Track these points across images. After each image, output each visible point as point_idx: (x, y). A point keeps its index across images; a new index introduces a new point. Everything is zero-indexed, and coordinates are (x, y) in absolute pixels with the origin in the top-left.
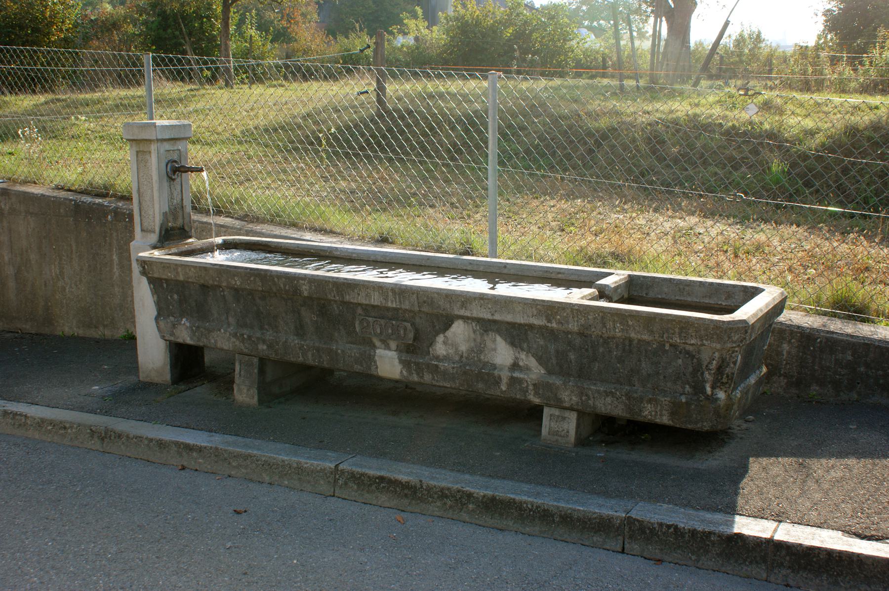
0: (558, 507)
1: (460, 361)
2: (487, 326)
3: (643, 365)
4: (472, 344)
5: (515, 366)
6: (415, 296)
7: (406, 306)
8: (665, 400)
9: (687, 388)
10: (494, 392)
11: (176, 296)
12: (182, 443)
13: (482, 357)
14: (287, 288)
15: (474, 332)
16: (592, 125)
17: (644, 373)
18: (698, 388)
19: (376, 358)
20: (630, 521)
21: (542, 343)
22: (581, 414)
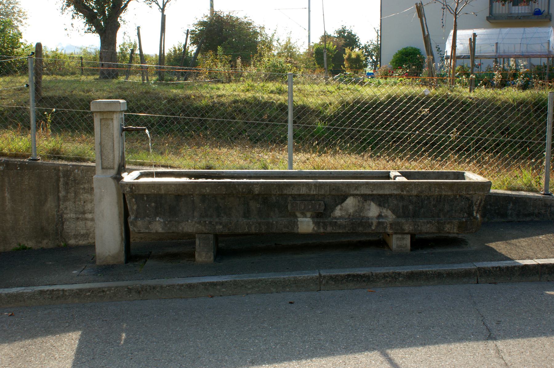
0: (445, 270)
1: (349, 218)
2: (366, 198)
3: (446, 207)
4: (357, 208)
5: (380, 216)
6: (328, 187)
7: (322, 192)
8: (456, 222)
9: (466, 215)
10: (368, 231)
11: (153, 204)
12: (208, 283)
13: (362, 214)
14: (244, 190)
15: (359, 202)
16: (197, 104)
17: (446, 211)
18: (470, 214)
19: (299, 223)
20: (479, 269)
21: (395, 202)
22: (413, 236)
